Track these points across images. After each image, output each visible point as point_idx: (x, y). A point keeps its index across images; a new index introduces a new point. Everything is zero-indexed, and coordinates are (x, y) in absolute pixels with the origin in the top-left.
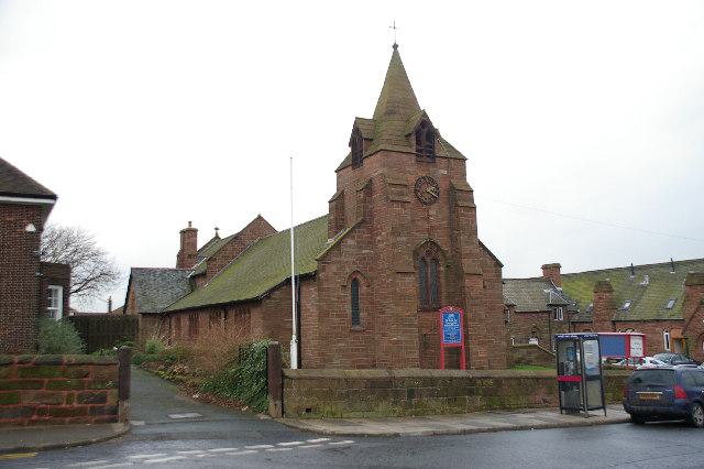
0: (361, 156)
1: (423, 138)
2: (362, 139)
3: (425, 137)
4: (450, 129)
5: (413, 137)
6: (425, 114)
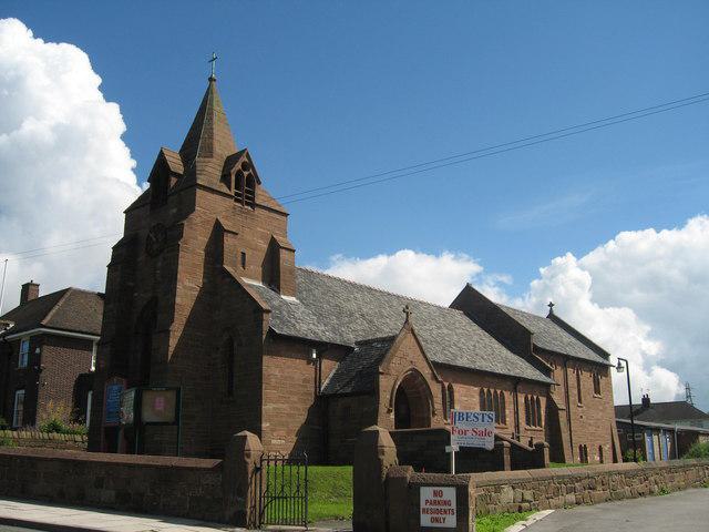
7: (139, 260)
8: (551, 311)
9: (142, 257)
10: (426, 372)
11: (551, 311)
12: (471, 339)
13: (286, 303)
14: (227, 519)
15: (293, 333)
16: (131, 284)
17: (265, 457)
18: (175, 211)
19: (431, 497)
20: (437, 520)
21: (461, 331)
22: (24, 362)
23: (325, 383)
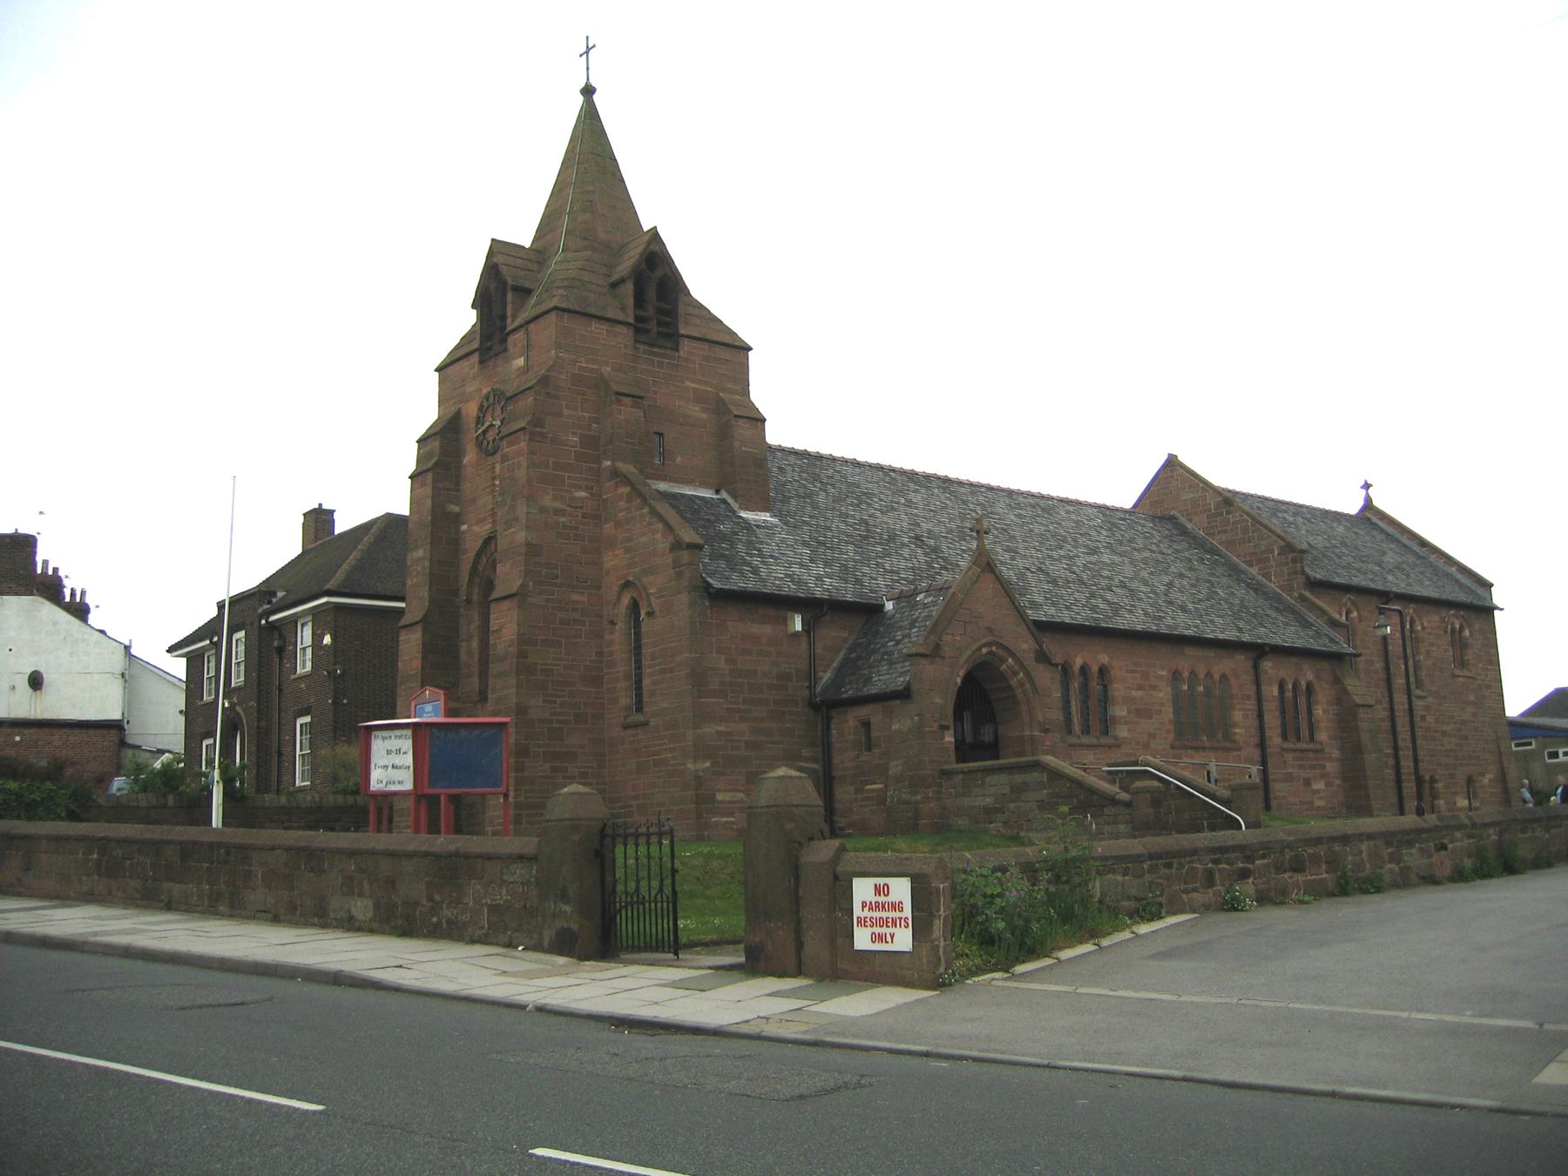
0: (505, 327)
1: (651, 293)
2: (504, 284)
3: (653, 291)
4: (707, 279)
5: (629, 288)
6: (654, 233)
7: (465, 461)
8: (1368, 500)
9: (470, 456)
10: (1025, 646)
11: (1368, 500)
12: (1165, 572)
13: (747, 526)
14: (546, 944)
15: (751, 585)
16: (455, 508)
17: (609, 831)
18: (521, 362)
19: (871, 897)
20: (880, 938)
21: (1147, 554)
22: (967, 716)
23: (826, 677)
